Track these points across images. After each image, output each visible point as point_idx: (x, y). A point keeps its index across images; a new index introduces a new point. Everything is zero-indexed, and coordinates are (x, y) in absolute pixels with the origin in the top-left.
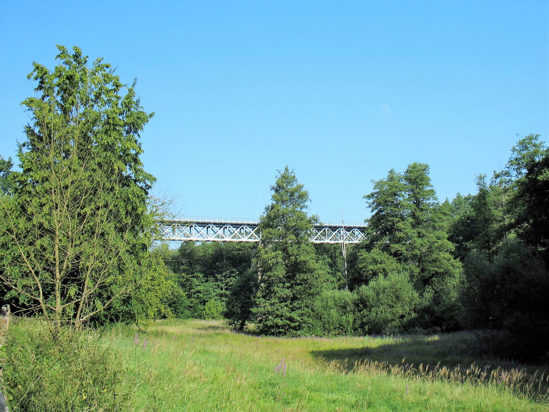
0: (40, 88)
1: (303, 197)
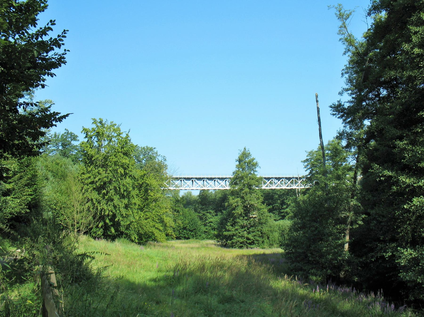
0: (86, 137)
1: (256, 165)
